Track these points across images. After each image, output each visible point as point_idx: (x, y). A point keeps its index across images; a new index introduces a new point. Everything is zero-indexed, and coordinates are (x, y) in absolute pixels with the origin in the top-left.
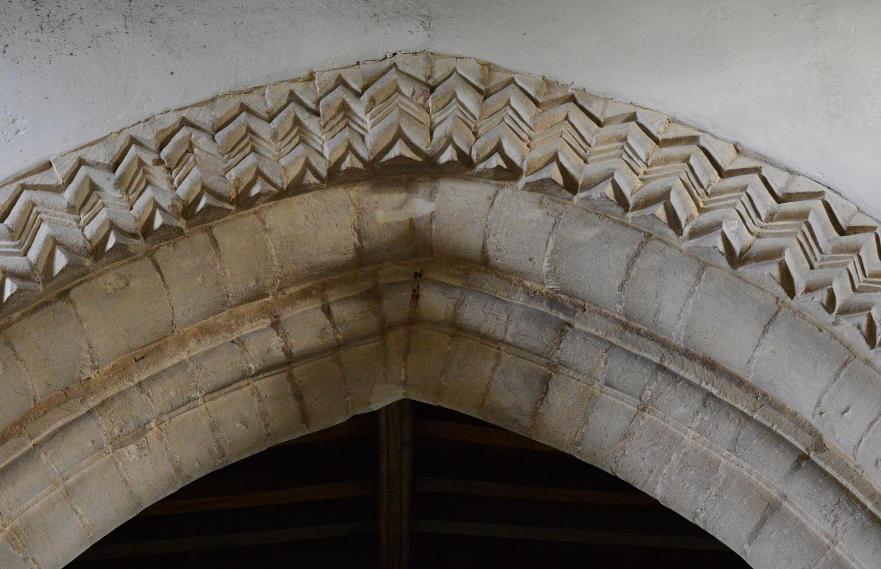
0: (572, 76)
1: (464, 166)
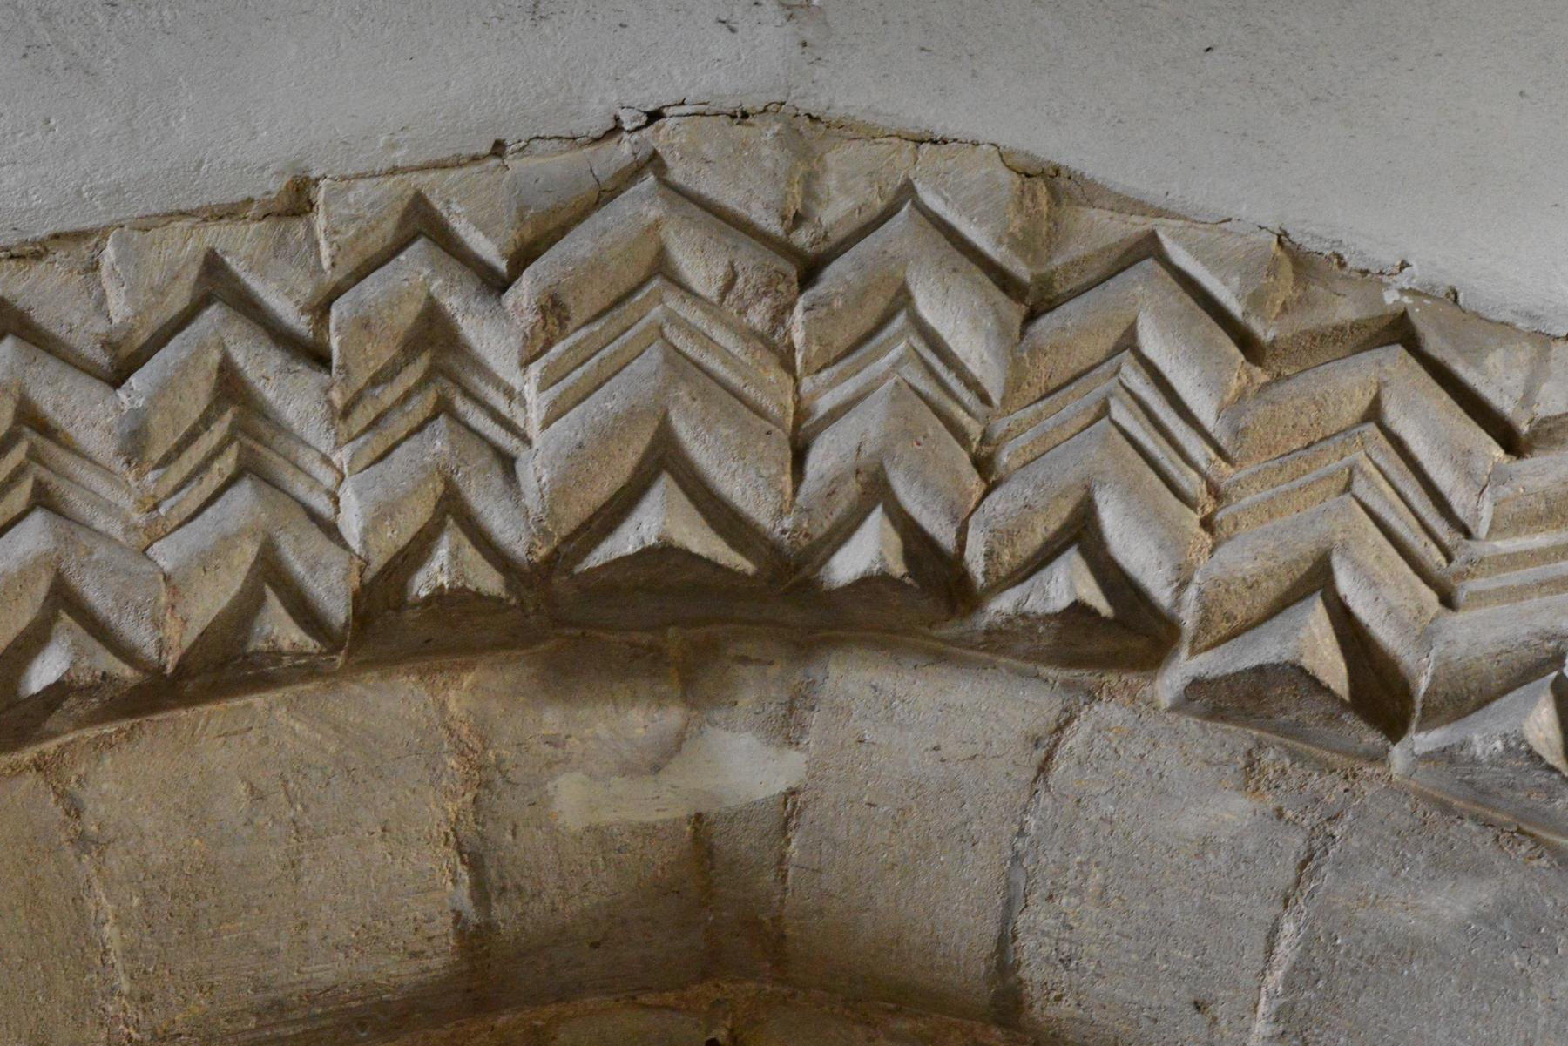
0: (1407, 237)
1: (933, 598)
